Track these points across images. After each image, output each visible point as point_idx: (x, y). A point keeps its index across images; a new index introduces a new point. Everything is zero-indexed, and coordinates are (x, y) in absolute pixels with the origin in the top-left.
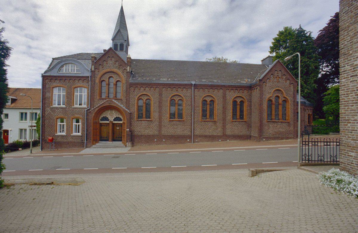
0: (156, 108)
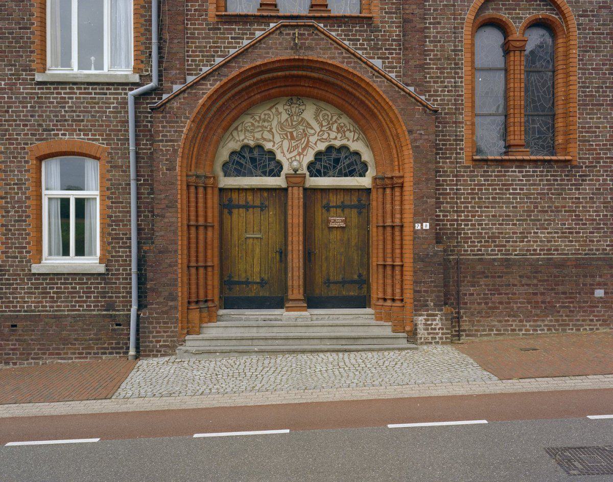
0: (596, 82)
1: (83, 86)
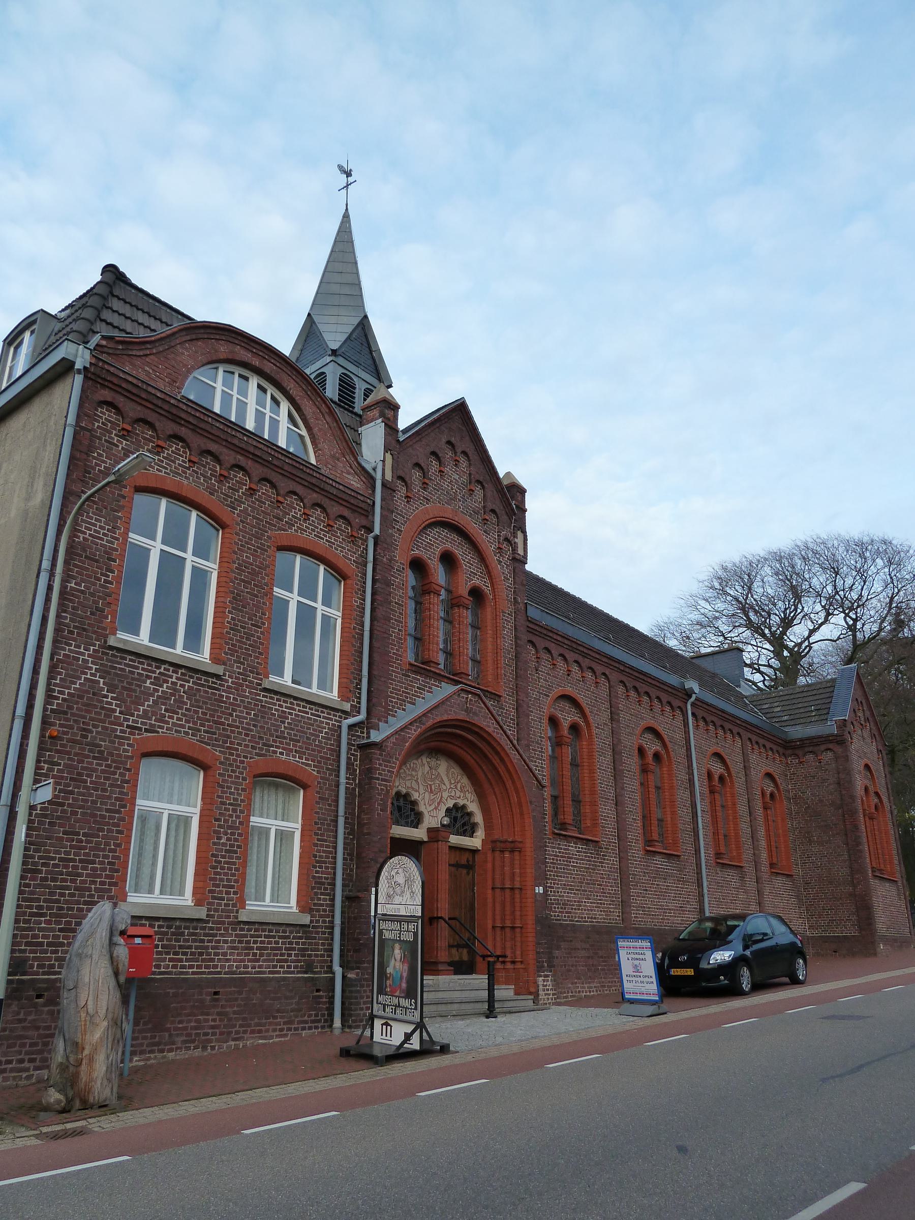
1: (302, 703)
